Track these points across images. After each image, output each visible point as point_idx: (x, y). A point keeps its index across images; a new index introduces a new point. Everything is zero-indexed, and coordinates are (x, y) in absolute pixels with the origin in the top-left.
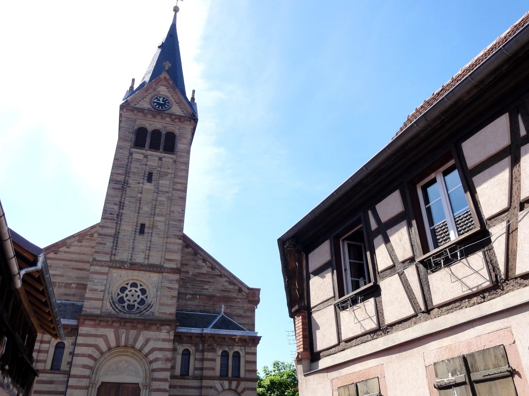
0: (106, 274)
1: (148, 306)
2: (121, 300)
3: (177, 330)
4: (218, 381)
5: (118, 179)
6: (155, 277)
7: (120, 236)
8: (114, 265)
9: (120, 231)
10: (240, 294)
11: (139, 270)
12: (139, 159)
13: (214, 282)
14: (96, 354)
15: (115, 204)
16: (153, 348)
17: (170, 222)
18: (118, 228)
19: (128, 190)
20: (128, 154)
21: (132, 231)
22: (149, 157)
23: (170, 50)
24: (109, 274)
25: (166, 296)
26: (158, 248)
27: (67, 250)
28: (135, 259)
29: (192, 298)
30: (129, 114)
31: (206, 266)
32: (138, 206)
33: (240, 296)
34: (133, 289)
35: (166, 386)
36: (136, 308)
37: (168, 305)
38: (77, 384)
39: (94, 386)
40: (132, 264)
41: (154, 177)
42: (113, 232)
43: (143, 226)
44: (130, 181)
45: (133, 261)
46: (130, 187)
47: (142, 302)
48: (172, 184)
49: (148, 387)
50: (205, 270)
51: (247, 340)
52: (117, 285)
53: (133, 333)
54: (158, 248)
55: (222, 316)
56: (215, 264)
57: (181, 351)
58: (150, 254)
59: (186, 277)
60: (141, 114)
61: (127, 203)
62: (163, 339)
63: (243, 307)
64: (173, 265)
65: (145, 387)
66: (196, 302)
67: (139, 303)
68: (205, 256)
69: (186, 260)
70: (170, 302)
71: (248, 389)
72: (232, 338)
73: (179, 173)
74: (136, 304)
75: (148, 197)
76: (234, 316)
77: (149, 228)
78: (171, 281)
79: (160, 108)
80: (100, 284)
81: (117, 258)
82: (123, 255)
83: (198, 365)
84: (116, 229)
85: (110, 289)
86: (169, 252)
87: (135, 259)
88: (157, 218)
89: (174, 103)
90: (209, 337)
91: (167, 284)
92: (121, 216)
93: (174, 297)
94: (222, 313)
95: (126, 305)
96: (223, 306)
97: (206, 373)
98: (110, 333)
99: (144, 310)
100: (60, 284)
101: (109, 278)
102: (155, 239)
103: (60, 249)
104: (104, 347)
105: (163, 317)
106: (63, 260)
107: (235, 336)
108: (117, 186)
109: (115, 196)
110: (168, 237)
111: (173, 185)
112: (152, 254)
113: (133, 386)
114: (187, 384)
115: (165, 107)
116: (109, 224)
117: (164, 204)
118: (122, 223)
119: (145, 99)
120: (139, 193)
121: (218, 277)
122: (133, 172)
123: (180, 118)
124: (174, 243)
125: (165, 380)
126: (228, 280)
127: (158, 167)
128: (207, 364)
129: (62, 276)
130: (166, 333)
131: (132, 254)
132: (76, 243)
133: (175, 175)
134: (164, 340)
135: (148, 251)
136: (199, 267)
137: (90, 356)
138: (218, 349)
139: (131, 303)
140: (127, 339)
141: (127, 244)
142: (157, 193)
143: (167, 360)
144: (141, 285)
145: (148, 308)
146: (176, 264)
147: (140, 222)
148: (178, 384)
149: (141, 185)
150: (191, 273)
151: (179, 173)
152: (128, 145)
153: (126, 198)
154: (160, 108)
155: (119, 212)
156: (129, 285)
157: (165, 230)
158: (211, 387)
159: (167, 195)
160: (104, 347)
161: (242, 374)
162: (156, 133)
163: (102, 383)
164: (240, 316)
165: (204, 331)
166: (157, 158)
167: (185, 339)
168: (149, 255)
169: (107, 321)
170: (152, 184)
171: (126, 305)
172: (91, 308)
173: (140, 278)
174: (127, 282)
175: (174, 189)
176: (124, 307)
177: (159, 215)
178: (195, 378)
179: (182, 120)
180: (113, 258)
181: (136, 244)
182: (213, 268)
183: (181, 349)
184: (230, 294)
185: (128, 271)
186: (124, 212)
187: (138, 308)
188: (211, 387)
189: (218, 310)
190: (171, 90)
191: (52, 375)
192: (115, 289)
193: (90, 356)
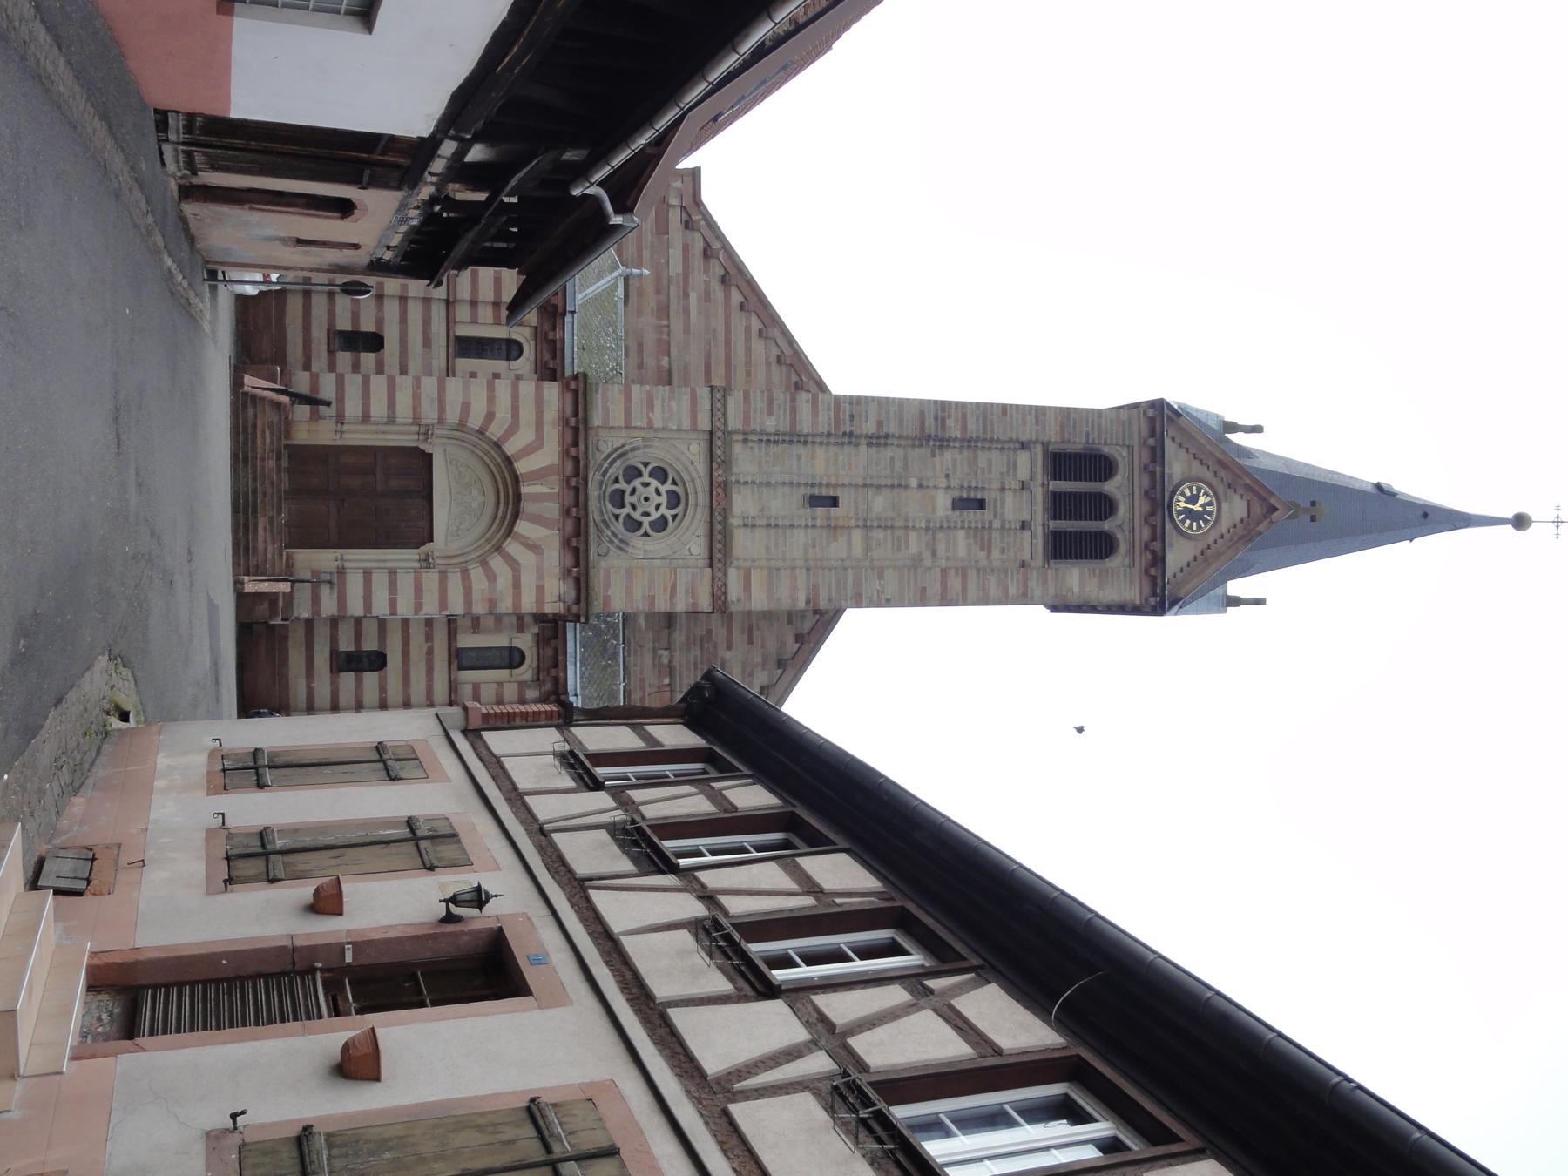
0: (694, 429)
2: (633, 473)
5: (950, 423)
6: (697, 548)
7: (797, 449)
12: (1015, 469)
15: (880, 424)
18: (818, 440)
19: (926, 451)
20: (1024, 438)
21: (814, 477)
22: (1026, 494)
23: (1381, 516)
34: (663, 499)
40: (725, 486)
41: (972, 516)
42: (805, 426)
43: (834, 502)
44: (948, 455)
46: (933, 455)
47: (633, 525)
53: (553, 510)
57: (517, 643)
59: (715, 647)
61: (888, 453)
70: (638, 593)
74: (627, 510)
75: (913, 504)
77: (829, 519)
78: (692, 590)
81: (738, 448)
82: (745, 462)
84: (814, 436)
88: (857, 536)
93: (652, 604)
98: (549, 455)
101: (684, 436)
102: (799, 538)
105: (597, 581)
110: (808, 569)
112: (760, 534)
117: (899, 549)
118: (833, 449)
119: (1196, 463)
122: (976, 458)
123: (1158, 560)
124: (794, 588)
129: (687, 330)
130: (554, 594)
133: (984, 570)
134: (540, 589)
135: (764, 522)
137: (490, 416)
139: (628, 499)
141: (776, 469)
142: (928, 529)
150: (728, 655)
152: (1052, 435)
155: (859, 437)
163: (431, 455)
166: (1026, 517)
167: (549, 652)
168: (754, 526)
171: (622, 485)
175: (944, 571)
176: (617, 481)
177: (867, 541)
178: (453, 687)
179: (1153, 571)
183: (525, 642)
187: (617, 517)
192: (657, 454)
193: (490, 416)
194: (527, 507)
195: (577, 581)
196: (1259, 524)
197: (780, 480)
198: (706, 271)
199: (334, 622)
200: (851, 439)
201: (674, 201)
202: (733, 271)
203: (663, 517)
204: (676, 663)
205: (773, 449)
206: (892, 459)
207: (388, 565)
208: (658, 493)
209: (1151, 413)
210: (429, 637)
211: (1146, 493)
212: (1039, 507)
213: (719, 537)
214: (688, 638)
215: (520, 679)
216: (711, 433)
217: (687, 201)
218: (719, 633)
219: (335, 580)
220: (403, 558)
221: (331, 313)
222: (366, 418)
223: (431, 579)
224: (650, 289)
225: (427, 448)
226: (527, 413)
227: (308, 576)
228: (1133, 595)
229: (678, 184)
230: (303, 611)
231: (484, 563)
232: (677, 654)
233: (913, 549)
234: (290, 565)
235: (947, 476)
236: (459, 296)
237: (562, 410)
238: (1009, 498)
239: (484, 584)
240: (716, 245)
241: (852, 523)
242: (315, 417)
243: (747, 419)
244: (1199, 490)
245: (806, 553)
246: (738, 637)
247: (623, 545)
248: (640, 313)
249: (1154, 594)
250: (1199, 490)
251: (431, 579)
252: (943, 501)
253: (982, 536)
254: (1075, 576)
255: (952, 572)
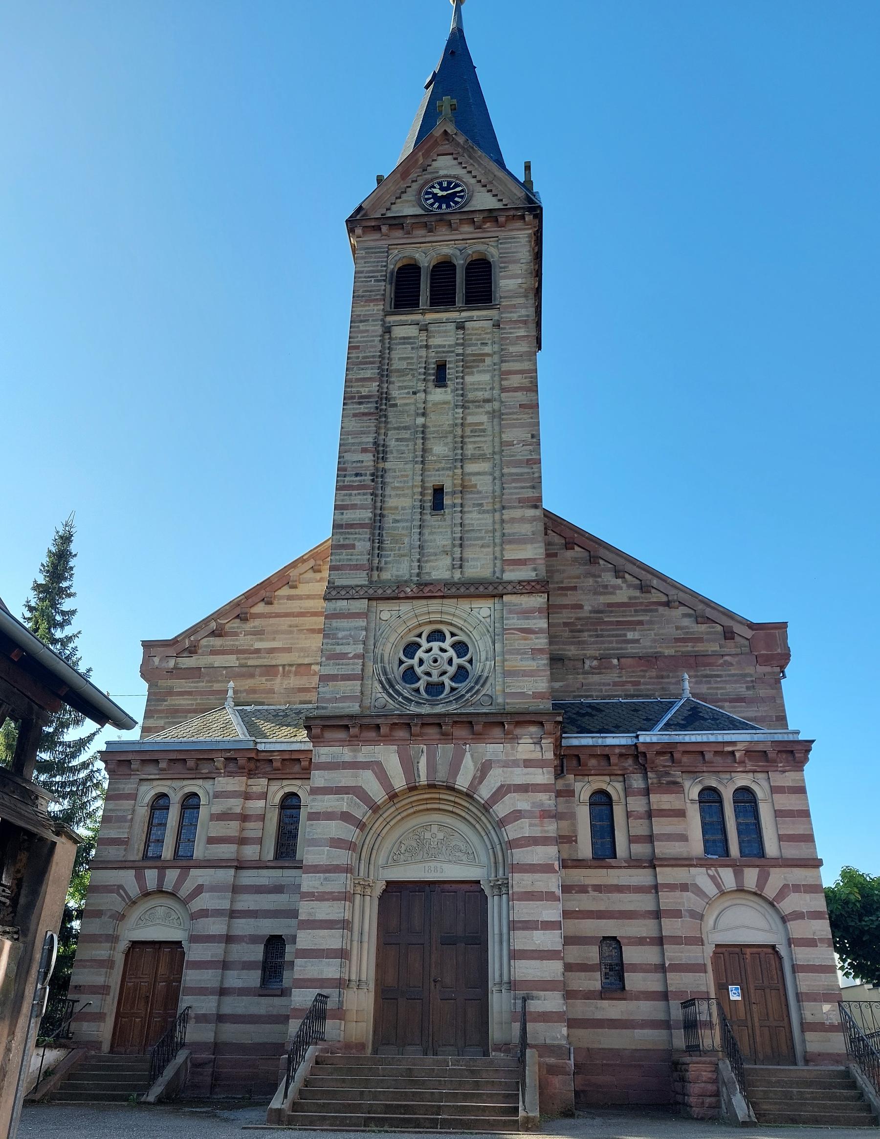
0: (365, 615)
1: (476, 683)
2: (410, 676)
3: (565, 743)
4: (703, 870)
5: (365, 391)
6: (484, 609)
7: (388, 522)
8: (380, 591)
9: (385, 512)
10: (730, 643)
11: (443, 597)
12: (409, 338)
13: (651, 622)
14: (360, 811)
15: (364, 450)
16: (502, 786)
17: (506, 470)
18: (379, 504)
19: (391, 412)
20: (380, 331)
21: (414, 507)
22: (432, 328)
23: (456, 80)
24: (372, 616)
25: (518, 652)
26: (482, 538)
27: (293, 592)
28: (429, 574)
29: (598, 668)
30: (372, 240)
31: (624, 586)
32: (419, 446)
33: (730, 647)
34: (435, 645)
35: (552, 883)
36: (447, 689)
37: (526, 674)
38: (321, 889)
39: (368, 891)
40: (421, 585)
41: (450, 372)
42: (366, 515)
43: (439, 491)
44: (395, 393)
45: (426, 578)
46: (395, 405)
47: (461, 674)
48: (497, 378)
49: (504, 890)
50: (622, 596)
51: (772, 755)
52: (392, 640)
53: (445, 751)
54: (482, 538)
55: (688, 699)
56: (650, 576)
57: (585, 796)
58: (465, 556)
59: (579, 619)
60: (399, 233)
61: (392, 443)
62: (525, 761)
63: (745, 675)
64: (526, 574)
65: (496, 891)
66: (612, 676)
67: (453, 679)
68: (620, 562)
69: (570, 578)
70: (530, 665)
71: (797, 888)
72: (725, 753)
73: (512, 349)
74: (446, 679)
75: (441, 420)
76: (725, 700)
77: (454, 493)
78: (526, 613)
79: (444, 206)
80: (351, 640)
81: (386, 576)
82: (399, 568)
83: (639, 828)
84: (375, 508)
85: (378, 651)
86: (510, 542)
87: (429, 574)
88: (470, 467)
89: (478, 187)
90: (660, 753)
91: (514, 622)
92: (382, 476)
93: (541, 651)
94: (687, 694)
95: (421, 685)
96: (686, 676)
97: (663, 849)
98: (388, 756)
99: (467, 692)
100: (287, 668)
101: (373, 625)
102: (473, 518)
103: (280, 593)
104: (378, 794)
105: (515, 704)
106: (287, 615)
107: (733, 743)
108: (363, 408)
109: (363, 433)
110: (503, 508)
111: (502, 379)
112: (469, 554)
113: (466, 887)
114: (615, 882)
115: (456, 203)
116: (357, 499)
117: (484, 431)
118: (388, 491)
119: (404, 197)
120: (418, 415)
121: (661, 609)
122: (398, 371)
123: (491, 215)
124: (522, 520)
125: (547, 868)
126: (691, 612)
127: (457, 344)
128: (660, 826)
129: (288, 650)
130: (531, 747)
131: (419, 561)
132: (310, 575)
133: (501, 356)
134: (528, 763)
135: (458, 550)
136: (606, 589)
137: (346, 817)
138: (687, 784)
139: (435, 678)
140: (432, 767)
141: (406, 540)
142: (463, 406)
143: (545, 814)
144: (453, 635)
145: (477, 687)
146: (535, 570)
147: (429, 485)
148: (588, 881)
149: (421, 395)
150: (587, 608)
151: (512, 349)
152: (376, 309)
153: (390, 433)
154: (444, 206)
155: (377, 469)
156: (424, 636)
157: (494, 491)
158: (684, 887)
159: (488, 407)
160: (378, 794)
161: (771, 848)
162: (444, 270)
163: (389, 883)
164: (740, 699)
165: (641, 739)
166: (453, 326)
167: (593, 762)
168: (461, 559)
169: (378, 727)
170: (449, 389)
171: (421, 685)
172: (336, 700)
173: (447, 618)
174: (417, 631)
175: (503, 390)
176: (417, 690)
177: (475, 459)
178: (634, 863)
179: (502, 219)
180: (375, 578)
181: (426, 537)
182: (644, 588)
183: (584, 789)
184: (700, 647)
185: (416, 602)
186: (388, 465)
187: (453, 689)
188: (684, 887)
189: (673, 689)
190: (464, 159)
191: (279, 872)
192: (390, 649)
193: (346, 817)
194: (442, 775)
195: (518, 724)
196: (458, 144)
197: (417, 537)
198: (236, 634)
199: (569, 995)
200: (379, 475)
201: (171, 663)
202: (237, 611)
203: (453, 646)
204: (597, 654)
205: (387, 544)
206: (397, 440)
207: (505, 930)
208: (429, 650)
209: (359, 231)
210: (583, 889)
211: (430, 231)
212: (444, 316)
213: (472, 589)
214: (572, 643)
215: (622, 794)
216: (369, 599)
217: (171, 652)
218: (566, 616)
219: (521, 993)
220: (496, 911)
221: (243, 992)
222: (343, 954)
223: (521, 882)
224: (249, 683)
225: (380, 887)
226: (344, 778)
227: (517, 1026)
228: (522, 236)
229: (156, 660)
230: (559, 1033)
231: (501, 823)
232: (589, 653)
233: (484, 418)
234: (504, 1047)
235: (414, 393)
236: (233, 856)
237: (342, 743)
238: (435, 341)
239: (525, 822)
240: (213, 625)
241: (459, 471)
242: (340, 1014)
243: (357, 567)
244: (427, 193)
245: (488, 512)
246: (570, 599)
247: (481, 681)
248: (272, 691)
249: (522, 217)
250: (427, 193)
251: (521, 882)
252: (438, 395)
253: (469, 364)
254: (509, 282)
255: (504, 383)
